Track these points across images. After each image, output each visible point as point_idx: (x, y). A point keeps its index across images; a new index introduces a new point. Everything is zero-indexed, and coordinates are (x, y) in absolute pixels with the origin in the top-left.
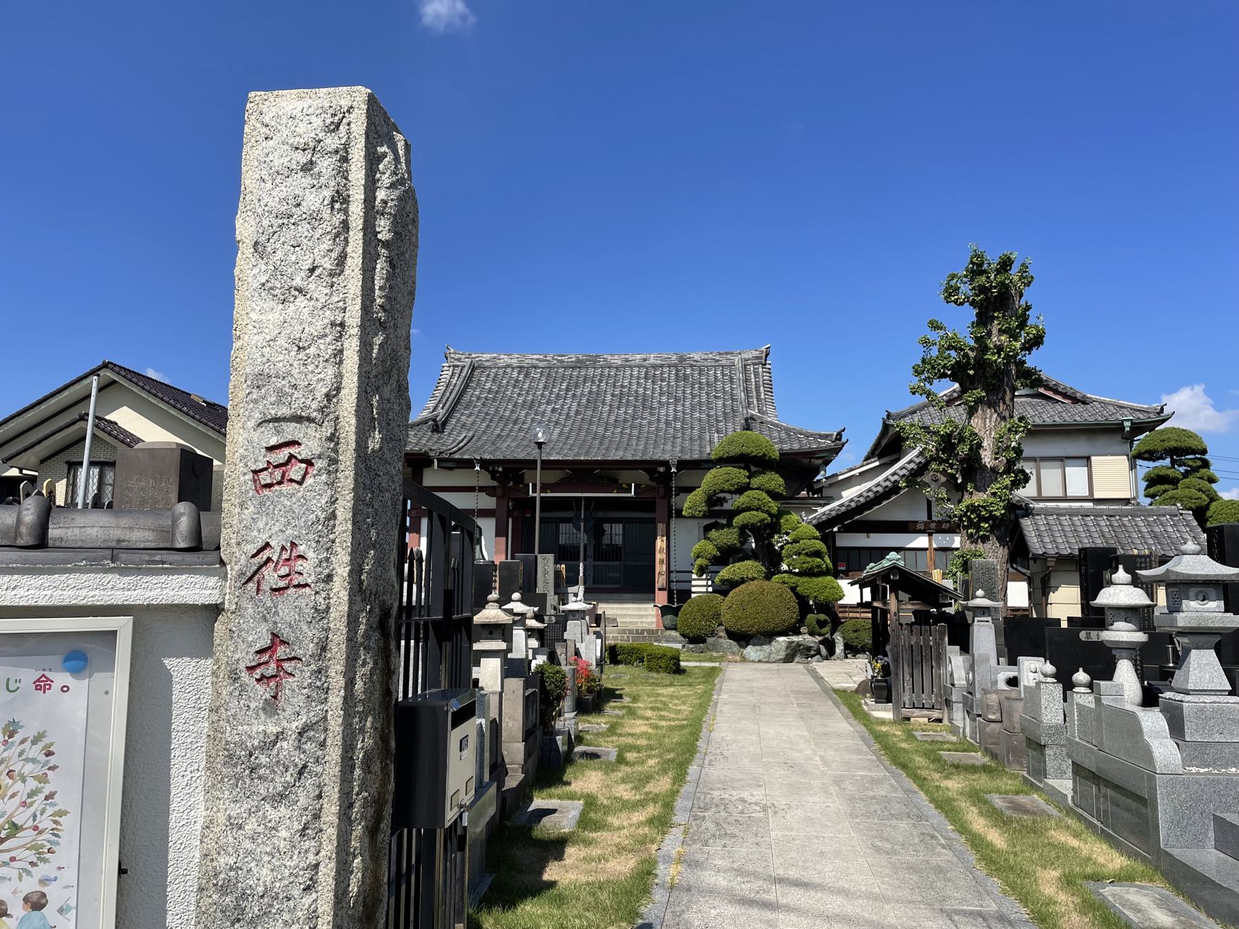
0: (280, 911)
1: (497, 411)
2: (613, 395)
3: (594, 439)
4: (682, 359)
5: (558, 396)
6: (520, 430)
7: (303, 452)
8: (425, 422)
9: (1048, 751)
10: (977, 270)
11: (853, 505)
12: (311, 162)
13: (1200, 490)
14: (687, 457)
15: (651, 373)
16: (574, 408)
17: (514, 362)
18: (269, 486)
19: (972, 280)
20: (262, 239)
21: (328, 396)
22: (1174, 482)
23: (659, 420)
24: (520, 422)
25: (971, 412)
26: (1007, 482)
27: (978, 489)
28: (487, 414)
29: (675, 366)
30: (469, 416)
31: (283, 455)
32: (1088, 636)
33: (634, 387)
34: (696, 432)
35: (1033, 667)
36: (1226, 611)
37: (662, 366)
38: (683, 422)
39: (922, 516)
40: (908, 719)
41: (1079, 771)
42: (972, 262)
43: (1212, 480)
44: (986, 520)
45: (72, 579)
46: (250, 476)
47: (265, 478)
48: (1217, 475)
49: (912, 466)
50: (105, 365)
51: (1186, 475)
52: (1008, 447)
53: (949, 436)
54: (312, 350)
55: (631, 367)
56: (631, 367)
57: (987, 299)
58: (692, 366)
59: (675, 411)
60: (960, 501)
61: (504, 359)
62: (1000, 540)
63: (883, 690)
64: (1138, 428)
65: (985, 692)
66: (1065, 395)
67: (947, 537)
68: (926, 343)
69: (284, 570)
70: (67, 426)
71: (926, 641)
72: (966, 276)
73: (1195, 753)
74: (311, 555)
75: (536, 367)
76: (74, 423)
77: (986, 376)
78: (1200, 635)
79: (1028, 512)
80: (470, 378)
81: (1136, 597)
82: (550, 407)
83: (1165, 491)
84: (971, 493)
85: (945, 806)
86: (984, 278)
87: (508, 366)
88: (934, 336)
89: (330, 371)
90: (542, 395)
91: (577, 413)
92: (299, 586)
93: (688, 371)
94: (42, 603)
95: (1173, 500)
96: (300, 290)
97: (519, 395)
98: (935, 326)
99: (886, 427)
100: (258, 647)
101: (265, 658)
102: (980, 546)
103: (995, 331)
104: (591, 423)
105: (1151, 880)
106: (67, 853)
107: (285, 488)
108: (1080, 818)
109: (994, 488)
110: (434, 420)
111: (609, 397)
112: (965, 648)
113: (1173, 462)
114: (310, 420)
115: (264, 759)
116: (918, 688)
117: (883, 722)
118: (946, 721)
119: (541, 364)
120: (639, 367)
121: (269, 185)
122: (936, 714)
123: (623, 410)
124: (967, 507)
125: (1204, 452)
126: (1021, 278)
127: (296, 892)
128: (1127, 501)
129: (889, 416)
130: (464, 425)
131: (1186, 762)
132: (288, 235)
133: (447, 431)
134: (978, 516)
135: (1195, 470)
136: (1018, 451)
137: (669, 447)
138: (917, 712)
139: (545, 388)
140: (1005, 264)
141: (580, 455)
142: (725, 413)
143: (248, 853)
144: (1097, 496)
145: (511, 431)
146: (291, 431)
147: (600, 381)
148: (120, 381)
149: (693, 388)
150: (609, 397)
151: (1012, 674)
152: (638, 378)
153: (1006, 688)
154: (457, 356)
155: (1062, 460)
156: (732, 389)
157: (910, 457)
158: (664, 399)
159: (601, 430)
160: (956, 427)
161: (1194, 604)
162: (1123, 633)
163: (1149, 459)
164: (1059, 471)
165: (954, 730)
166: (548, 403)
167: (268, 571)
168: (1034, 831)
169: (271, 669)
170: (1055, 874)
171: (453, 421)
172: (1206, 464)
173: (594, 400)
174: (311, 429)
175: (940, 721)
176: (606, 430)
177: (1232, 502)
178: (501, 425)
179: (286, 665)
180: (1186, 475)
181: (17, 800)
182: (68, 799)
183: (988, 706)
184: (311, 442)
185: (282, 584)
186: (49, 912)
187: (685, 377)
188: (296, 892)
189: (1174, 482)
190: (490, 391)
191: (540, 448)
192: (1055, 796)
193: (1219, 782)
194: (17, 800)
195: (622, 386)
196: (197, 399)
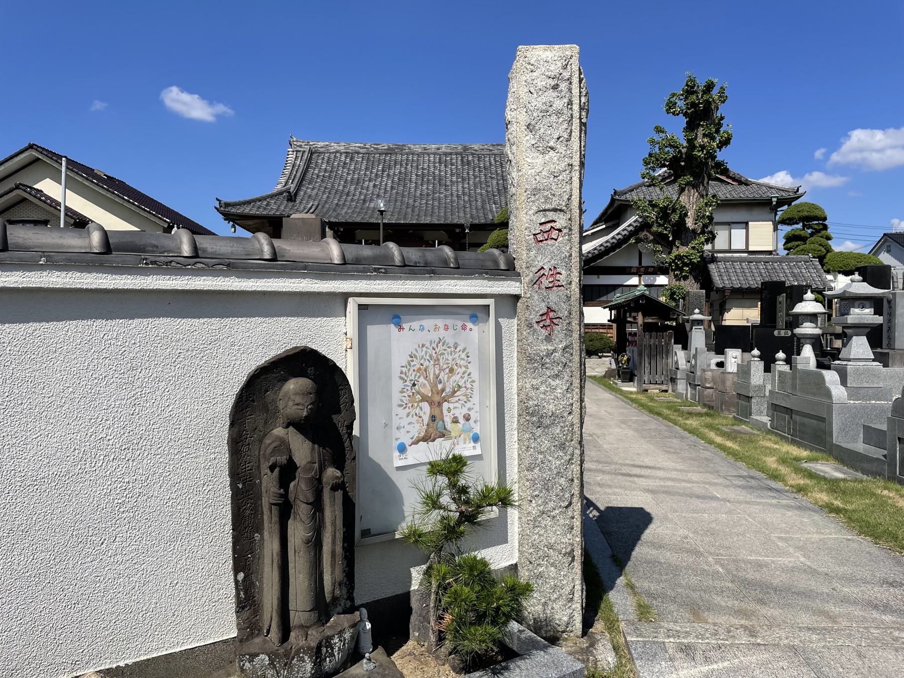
0: (559, 422)
1: (333, 186)
2: (417, 175)
3: (407, 207)
4: (465, 149)
5: (377, 175)
6: (352, 200)
7: (557, 225)
8: (281, 193)
9: (753, 400)
10: (690, 91)
11: (590, 255)
12: (557, 85)
13: (821, 245)
14: (476, 222)
15: (443, 158)
16: (389, 185)
17: (342, 149)
18: (541, 241)
19: (686, 98)
20: (533, 123)
21: (569, 199)
22: (803, 239)
23: (452, 195)
24: (351, 194)
25: (682, 190)
26: (703, 239)
27: (682, 244)
28: (326, 188)
29: (461, 154)
30: (313, 189)
31: (548, 226)
32: (779, 333)
33: (432, 169)
34: (479, 204)
35: (734, 355)
36: (875, 314)
37: (451, 154)
38: (469, 196)
39: (636, 263)
40: (647, 391)
41: (775, 408)
42: (687, 85)
43: (828, 238)
44: (685, 264)
45: (474, 282)
46: (532, 237)
47: (540, 237)
48: (832, 235)
49: (631, 228)
50: (31, 147)
51: (812, 235)
52: (703, 216)
53: (666, 208)
54: (560, 177)
55: (428, 154)
56: (428, 154)
57: (695, 112)
58: (472, 154)
59: (463, 187)
60: (670, 253)
61: (334, 147)
62: (696, 279)
63: (628, 375)
64: (781, 202)
65: (704, 371)
66: (734, 179)
67: (652, 277)
68: (652, 142)
69: (551, 279)
70: (7, 193)
71: (660, 342)
72: (682, 95)
73: (854, 393)
74: (563, 272)
75: (358, 153)
76: (11, 191)
77: (691, 166)
78: (859, 328)
79: (713, 260)
80: (310, 160)
81: (817, 308)
82: (372, 184)
83: (798, 246)
84: (678, 247)
85: (692, 431)
86: (695, 97)
87: (337, 152)
88: (657, 137)
89: (568, 187)
90: (365, 174)
91: (392, 188)
92: (559, 286)
93: (470, 158)
94: (465, 292)
95: (804, 252)
96: (552, 148)
97: (348, 174)
98: (659, 130)
99: (613, 200)
100: (541, 313)
101: (544, 318)
102: (682, 283)
103: (700, 135)
104: (403, 196)
105: (827, 460)
106: (476, 399)
107: (549, 242)
108: (777, 434)
109: (694, 243)
110: (289, 192)
111: (414, 177)
112: (685, 347)
113: (804, 226)
114: (561, 210)
115: (548, 361)
116: (653, 371)
117: (631, 393)
118: (670, 391)
119: (362, 151)
120: (434, 154)
121: (535, 95)
122: (664, 387)
123: (425, 187)
124: (676, 256)
125: (825, 219)
126: (720, 96)
127: (566, 415)
128: (770, 253)
129: (615, 193)
130: (310, 196)
131: (850, 397)
132: (545, 121)
133: (298, 201)
134: (683, 262)
135: (818, 231)
136: (711, 218)
137: (462, 215)
138: (652, 386)
139: (367, 169)
140: (709, 87)
141: (400, 219)
142: (498, 190)
143: (542, 399)
144: (751, 249)
145: (345, 201)
146: (551, 215)
147: (407, 165)
148: (41, 160)
149: (474, 171)
150: (414, 177)
151: (719, 360)
152: (434, 163)
153: (715, 368)
154: (299, 144)
155: (729, 224)
156: (502, 172)
157: (631, 221)
158: (454, 179)
159: (411, 201)
160: (671, 202)
161: (857, 310)
162: (808, 329)
163: (788, 224)
164: (727, 232)
165: (679, 395)
166: (370, 180)
167: (543, 279)
168: (752, 442)
169: (548, 322)
170: (775, 458)
171: (302, 193)
172: (825, 227)
173: (403, 179)
174: (561, 215)
175: (667, 391)
176: (415, 201)
177: (841, 253)
178: (338, 196)
179: (554, 321)
180: (812, 235)
181: (459, 376)
182: (475, 376)
183: (706, 379)
184: (561, 221)
185: (550, 285)
186: (471, 421)
187: (468, 163)
188: (566, 415)
189: (803, 239)
190: (326, 170)
191: (382, 214)
192: (760, 426)
193: (867, 408)
194: (459, 376)
195: (423, 169)
196: (99, 173)
